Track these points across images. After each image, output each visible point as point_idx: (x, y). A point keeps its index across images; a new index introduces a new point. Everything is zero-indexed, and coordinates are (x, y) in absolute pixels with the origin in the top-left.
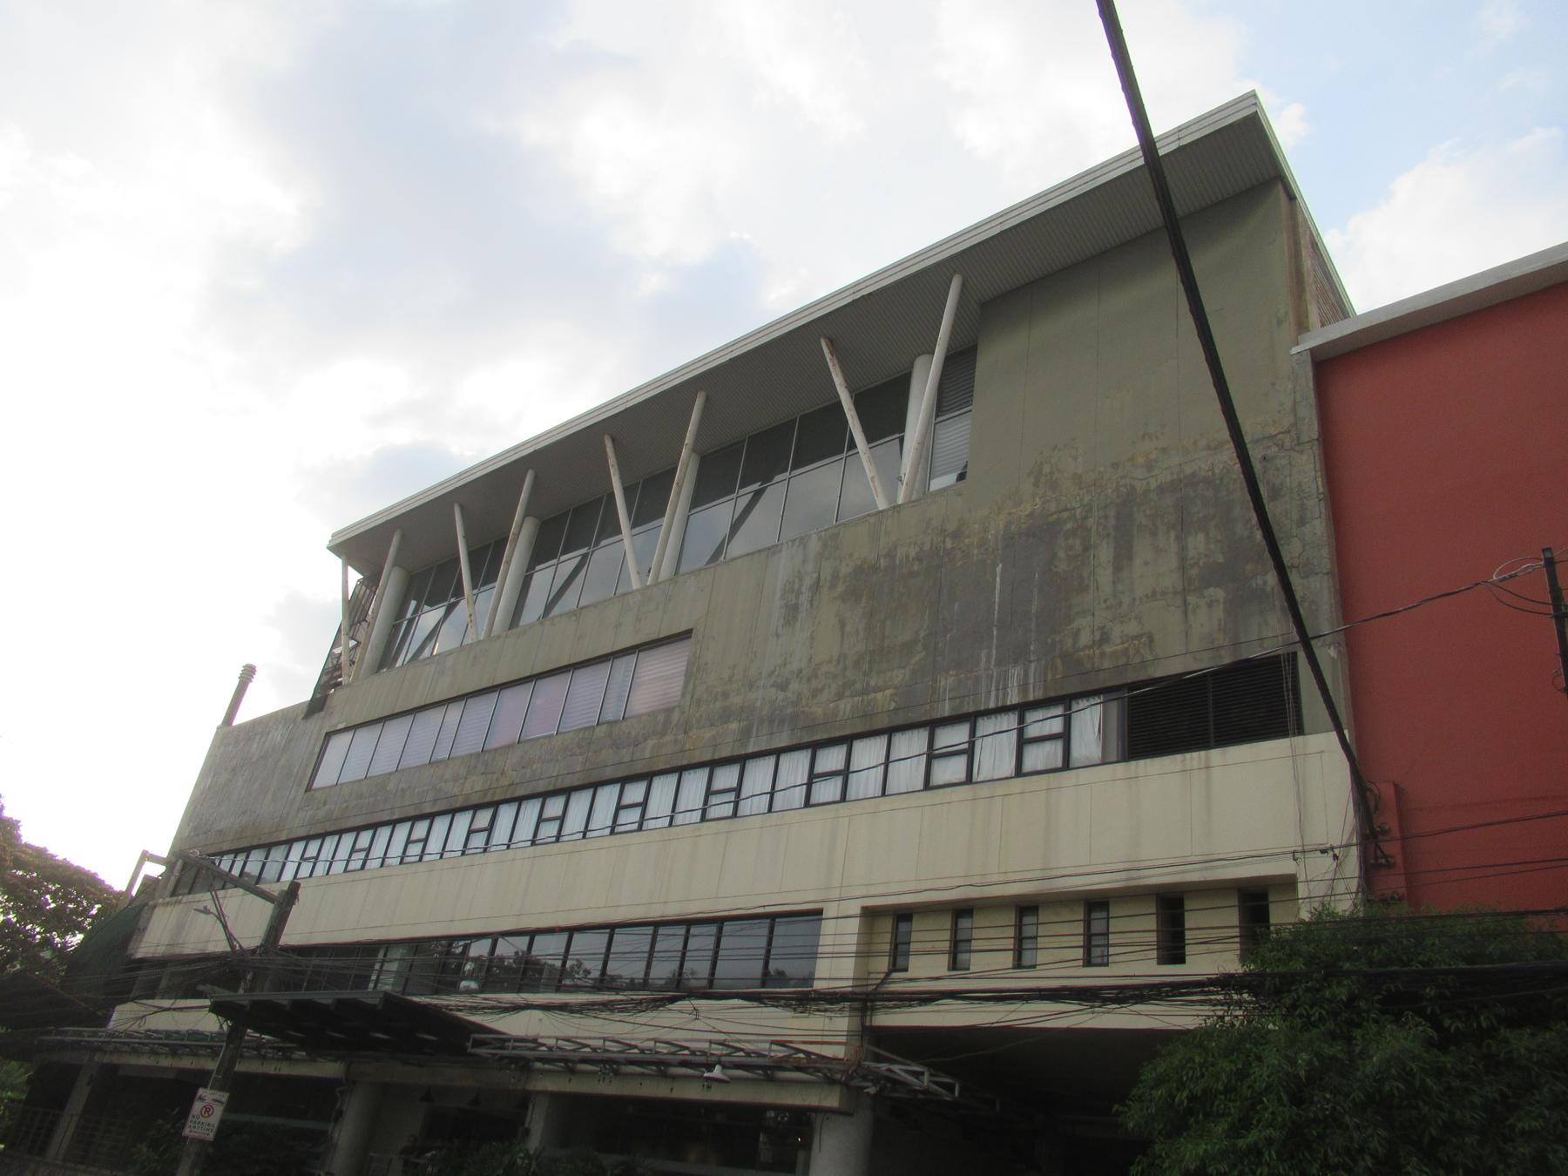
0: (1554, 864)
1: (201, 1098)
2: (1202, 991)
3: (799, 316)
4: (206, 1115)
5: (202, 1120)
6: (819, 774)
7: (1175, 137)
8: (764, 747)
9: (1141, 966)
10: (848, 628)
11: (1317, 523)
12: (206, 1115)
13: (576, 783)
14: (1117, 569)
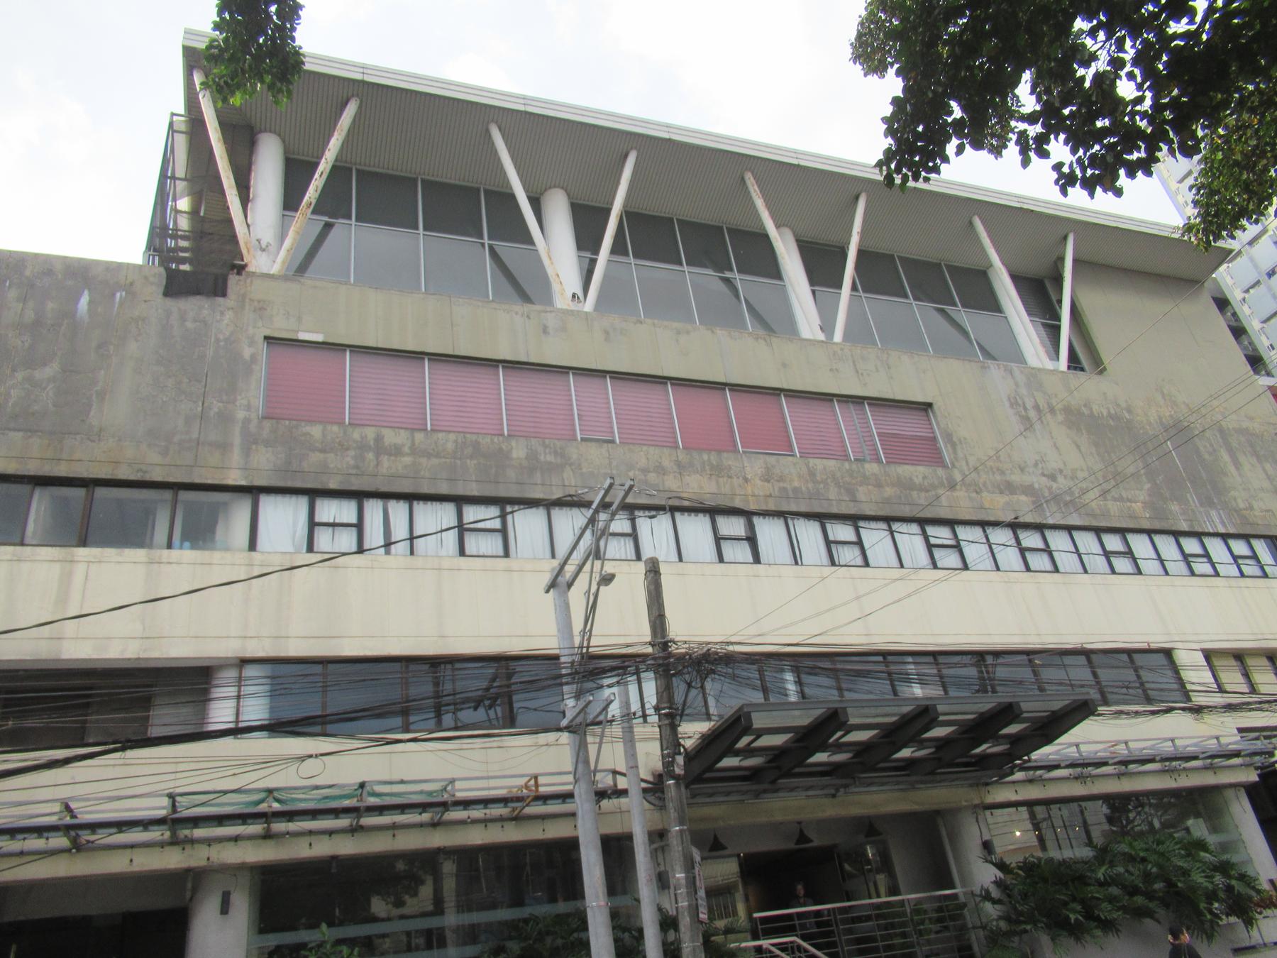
14: (1237, 469)
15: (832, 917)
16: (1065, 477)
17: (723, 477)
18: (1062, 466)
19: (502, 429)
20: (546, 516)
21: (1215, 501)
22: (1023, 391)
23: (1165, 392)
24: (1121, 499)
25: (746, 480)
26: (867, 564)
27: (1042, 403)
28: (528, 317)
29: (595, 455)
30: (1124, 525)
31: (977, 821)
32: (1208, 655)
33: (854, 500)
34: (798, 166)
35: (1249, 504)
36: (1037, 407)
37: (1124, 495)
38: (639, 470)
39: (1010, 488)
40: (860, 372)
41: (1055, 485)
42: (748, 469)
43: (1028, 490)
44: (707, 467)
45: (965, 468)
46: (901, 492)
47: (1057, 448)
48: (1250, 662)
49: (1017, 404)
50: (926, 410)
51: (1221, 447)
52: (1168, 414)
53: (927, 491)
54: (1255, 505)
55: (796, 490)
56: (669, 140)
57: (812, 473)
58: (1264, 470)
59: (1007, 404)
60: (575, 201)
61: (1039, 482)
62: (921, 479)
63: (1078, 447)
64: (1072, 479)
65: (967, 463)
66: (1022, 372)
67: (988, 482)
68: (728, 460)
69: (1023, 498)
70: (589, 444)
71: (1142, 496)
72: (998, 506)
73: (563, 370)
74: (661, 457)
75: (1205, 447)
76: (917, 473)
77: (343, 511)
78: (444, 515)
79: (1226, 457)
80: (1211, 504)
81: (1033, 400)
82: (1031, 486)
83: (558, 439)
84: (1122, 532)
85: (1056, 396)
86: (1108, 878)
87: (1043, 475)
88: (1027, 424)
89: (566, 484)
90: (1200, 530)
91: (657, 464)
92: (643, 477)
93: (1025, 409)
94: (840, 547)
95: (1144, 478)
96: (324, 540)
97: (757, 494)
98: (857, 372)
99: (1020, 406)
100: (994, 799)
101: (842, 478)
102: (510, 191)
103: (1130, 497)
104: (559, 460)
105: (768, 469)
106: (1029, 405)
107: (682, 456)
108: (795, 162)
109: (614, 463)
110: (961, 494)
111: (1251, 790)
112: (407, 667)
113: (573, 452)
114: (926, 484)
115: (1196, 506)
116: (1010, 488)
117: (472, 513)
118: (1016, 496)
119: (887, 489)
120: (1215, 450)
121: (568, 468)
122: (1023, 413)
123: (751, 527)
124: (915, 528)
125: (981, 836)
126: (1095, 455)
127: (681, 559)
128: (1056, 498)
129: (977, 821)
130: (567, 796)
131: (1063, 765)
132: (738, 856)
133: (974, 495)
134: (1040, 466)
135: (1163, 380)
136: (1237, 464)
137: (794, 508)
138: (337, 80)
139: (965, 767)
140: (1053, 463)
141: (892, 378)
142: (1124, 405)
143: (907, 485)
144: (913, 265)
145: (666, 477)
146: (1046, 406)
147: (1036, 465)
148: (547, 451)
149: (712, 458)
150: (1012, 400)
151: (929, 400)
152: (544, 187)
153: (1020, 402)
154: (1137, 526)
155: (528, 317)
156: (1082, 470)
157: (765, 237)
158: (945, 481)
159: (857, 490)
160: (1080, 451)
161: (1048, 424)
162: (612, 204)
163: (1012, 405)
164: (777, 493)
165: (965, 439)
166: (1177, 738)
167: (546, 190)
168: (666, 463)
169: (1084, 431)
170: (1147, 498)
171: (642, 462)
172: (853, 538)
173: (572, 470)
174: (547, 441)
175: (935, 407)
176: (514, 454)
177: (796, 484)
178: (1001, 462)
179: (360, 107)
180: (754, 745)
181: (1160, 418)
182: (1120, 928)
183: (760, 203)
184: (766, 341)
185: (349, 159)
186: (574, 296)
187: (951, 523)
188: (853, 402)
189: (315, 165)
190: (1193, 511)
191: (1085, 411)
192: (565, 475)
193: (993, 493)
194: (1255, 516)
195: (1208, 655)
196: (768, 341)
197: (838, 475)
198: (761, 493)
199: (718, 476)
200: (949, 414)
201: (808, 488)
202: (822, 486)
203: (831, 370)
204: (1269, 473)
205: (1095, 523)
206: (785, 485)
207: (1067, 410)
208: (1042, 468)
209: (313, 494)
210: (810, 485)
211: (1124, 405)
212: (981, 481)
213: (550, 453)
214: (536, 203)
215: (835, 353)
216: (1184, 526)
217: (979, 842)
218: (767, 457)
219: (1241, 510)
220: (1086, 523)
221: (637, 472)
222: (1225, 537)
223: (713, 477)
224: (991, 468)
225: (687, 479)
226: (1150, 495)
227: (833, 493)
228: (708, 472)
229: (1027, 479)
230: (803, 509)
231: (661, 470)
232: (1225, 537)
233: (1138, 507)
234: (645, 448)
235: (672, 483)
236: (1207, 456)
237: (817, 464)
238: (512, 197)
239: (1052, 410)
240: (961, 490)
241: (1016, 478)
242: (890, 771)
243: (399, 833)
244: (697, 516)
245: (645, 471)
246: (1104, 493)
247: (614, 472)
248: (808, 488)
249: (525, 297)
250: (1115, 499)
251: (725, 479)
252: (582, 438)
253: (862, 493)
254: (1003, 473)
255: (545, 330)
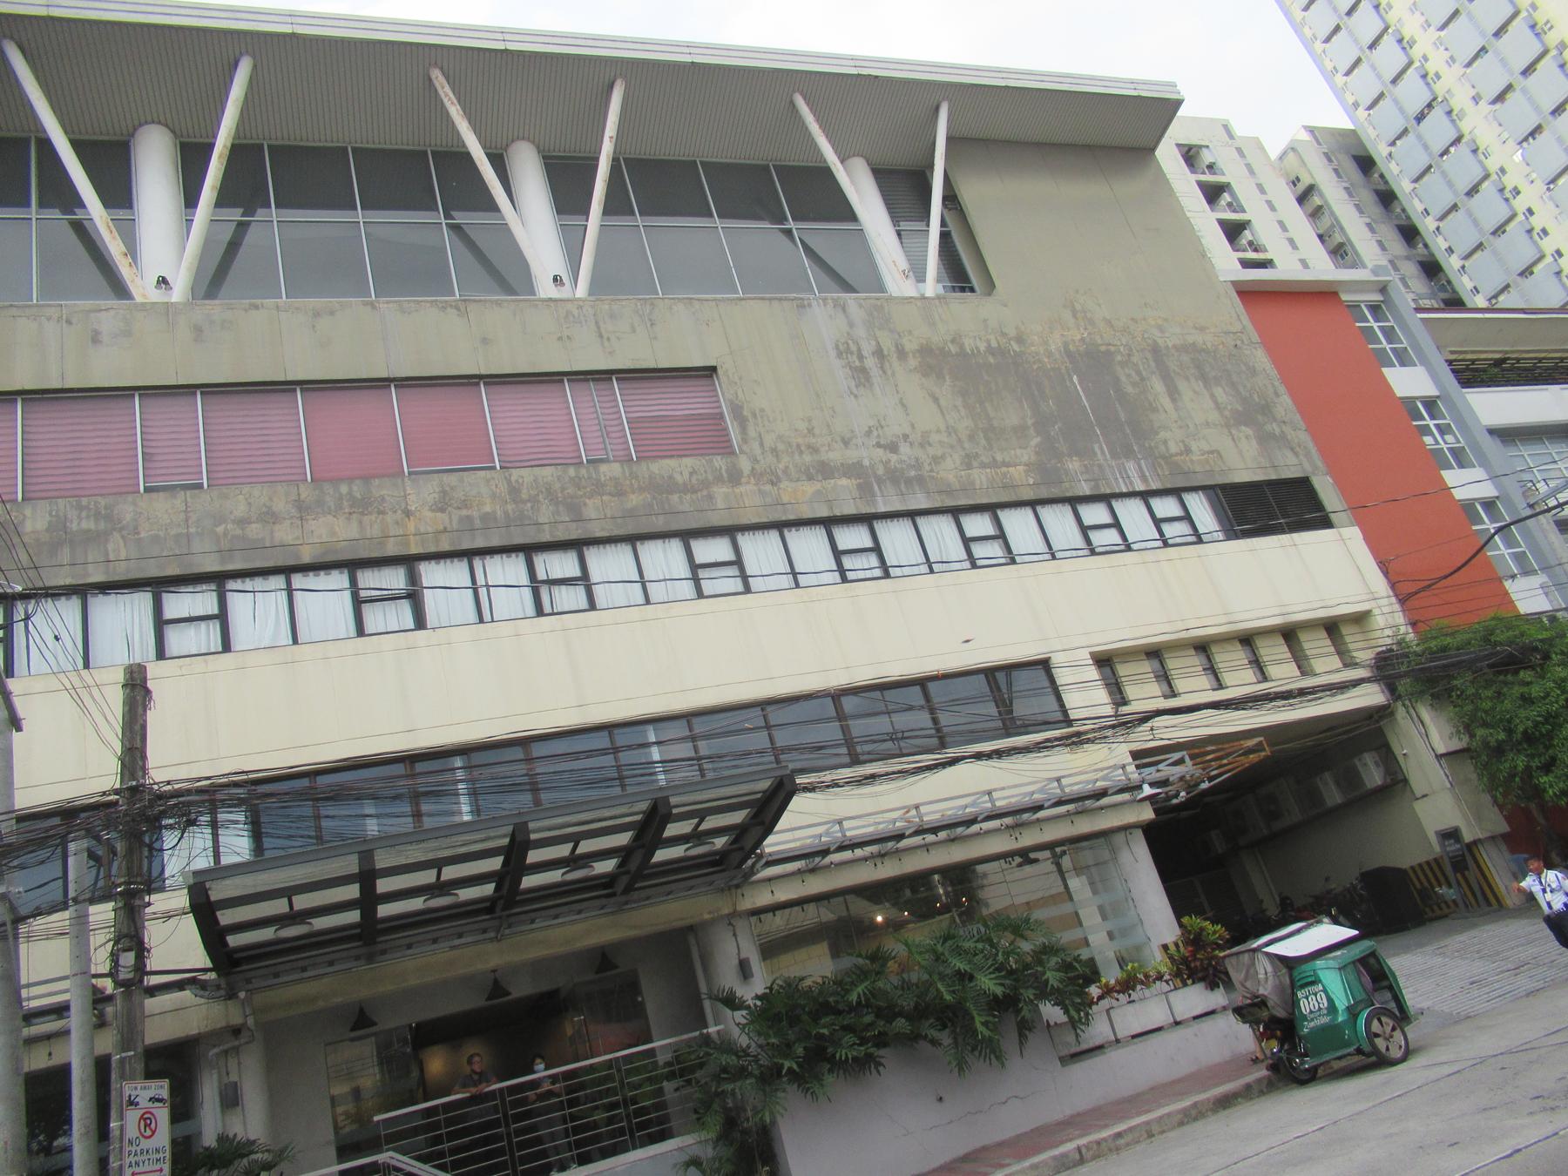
0: (79, 702)
1: (132, 1103)
2: (47, 831)
3: (758, 56)
4: (148, 1133)
5: (145, 1144)
6: (690, 547)
7: (1132, 86)
8: (897, 506)
9: (1240, 681)
10: (943, 402)
11: (1285, 397)
12: (148, 1133)
13: (599, 534)
14: (1174, 400)
15: (614, 1071)
16: (911, 444)
17: (370, 513)
18: (908, 430)
19: (581, 457)
20: (779, 539)
21: (1135, 448)
22: (861, 332)
23: (1078, 307)
24: (994, 464)
25: (408, 513)
26: (648, 602)
27: (887, 344)
28: (69, 322)
29: (163, 509)
30: (994, 500)
31: (735, 935)
32: (1104, 661)
33: (579, 519)
34: (506, 51)
35: (1186, 446)
36: (879, 353)
37: (999, 458)
38: (233, 522)
39: (825, 471)
40: (605, 336)
41: (894, 458)
42: (412, 498)
43: (853, 469)
44: (345, 503)
45: (758, 451)
46: (654, 498)
47: (903, 405)
48: (1123, 670)
49: (848, 351)
50: (711, 376)
51: (1153, 373)
52: (1079, 337)
53: (695, 492)
54: (1194, 446)
55: (485, 517)
56: (293, 35)
57: (514, 490)
58: (1212, 396)
59: (833, 354)
60: (778, 163)
61: (868, 454)
62: (686, 476)
63: (936, 400)
64: (922, 445)
65: (762, 445)
66: (861, 306)
67: (791, 466)
68: (383, 490)
69: (844, 482)
70: (154, 495)
71: (1027, 455)
72: (803, 497)
73: (122, 393)
74: (271, 499)
75: (1129, 376)
76: (681, 468)
77: (201, 601)
78: (511, 570)
79: (1158, 386)
80: (1129, 453)
81: (874, 343)
82: (859, 464)
83: (101, 495)
84: (991, 509)
85: (910, 332)
86: (863, 999)
87: (879, 445)
88: (861, 375)
89: (112, 557)
90: (1108, 491)
91: (264, 509)
92: (239, 532)
93: (861, 357)
94: (556, 589)
95: (1032, 432)
96: (178, 640)
97: (422, 530)
98: (601, 336)
99: (852, 353)
100: (754, 903)
101: (563, 489)
102: (463, 150)
103: (1007, 460)
104: (102, 526)
105: (444, 493)
106: (867, 348)
107: (306, 493)
108: (500, 46)
109: (194, 517)
110: (747, 489)
111: (1149, 830)
112: (412, 768)
113: (126, 510)
114: (694, 481)
115: (1106, 460)
116: (825, 471)
117: (371, 580)
118: (832, 481)
119: (632, 497)
120: (1143, 379)
121: (116, 535)
122: (857, 363)
123: (998, 523)
124: (1066, 510)
125: (739, 954)
126: (961, 408)
127: (295, 641)
128: (895, 477)
129: (735, 935)
130: (61, 1010)
131: (907, 834)
132: (410, 1026)
133: (768, 487)
134: (875, 433)
135: (1077, 292)
136: (1173, 393)
137: (480, 543)
138: (457, 51)
139: (713, 867)
140: (896, 425)
141: (655, 338)
142: (1013, 333)
143: (668, 486)
144: (718, 171)
145: (277, 527)
146: (893, 349)
147: (869, 433)
148: (84, 514)
149: (355, 488)
150: (841, 347)
151: (713, 363)
152: (510, 137)
153: (854, 348)
154: (1013, 498)
155: (69, 322)
156: (938, 431)
157: (826, 173)
158: (725, 475)
159: (585, 504)
160: (939, 406)
161: (893, 374)
162: (215, 137)
163: (840, 355)
164: (455, 526)
165: (762, 410)
166: (995, 790)
167: (135, 129)
168: (280, 505)
169: (947, 377)
170: (1033, 458)
171: (240, 510)
172: (869, 543)
173: (123, 537)
174: (84, 501)
175: (720, 371)
176: (28, 527)
177: (488, 509)
178: (814, 435)
179: (255, 67)
180: (701, 828)
181: (1066, 345)
182: (882, 1060)
183: (455, 111)
184: (459, 310)
185: (439, 142)
186: (555, 279)
187: (991, 509)
188: (593, 380)
189: (211, 146)
190: (1100, 466)
191: (953, 349)
192: (111, 547)
193: (798, 480)
194: (1192, 461)
195: (1104, 661)
196: (463, 309)
197: (557, 486)
198: (430, 530)
199: (362, 514)
200: (740, 379)
201: (506, 513)
202: (529, 505)
203: (560, 339)
204: (1220, 400)
205: (950, 503)
206: (469, 513)
207: (925, 351)
208: (878, 436)
209: (159, 586)
210: (510, 507)
211: (1013, 333)
212: (781, 466)
213: (88, 517)
214: (499, 162)
215: (568, 313)
216: (1085, 489)
217: (736, 962)
218: (445, 477)
219: (1171, 456)
220: (938, 505)
221: (230, 526)
222: (1145, 496)
223: (354, 516)
224: (798, 446)
225: (312, 524)
226: (1037, 453)
227: (545, 514)
228: (347, 510)
229: (852, 455)
230: (495, 542)
231: (270, 517)
232: (1145, 496)
233: (1017, 473)
234: (246, 489)
235: (285, 533)
236: (1130, 389)
237: (524, 476)
238: (467, 156)
239: (902, 354)
240: (748, 483)
241: (835, 456)
242: (597, 890)
243: (1045, 827)
244: (318, 575)
245: (243, 522)
246: (968, 461)
247: (192, 530)
248: (506, 513)
249: (508, 289)
250: (983, 466)
251: (373, 517)
252: (145, 488)
253: (592, 508)
254: (814, 450)
255: (96, 338)
